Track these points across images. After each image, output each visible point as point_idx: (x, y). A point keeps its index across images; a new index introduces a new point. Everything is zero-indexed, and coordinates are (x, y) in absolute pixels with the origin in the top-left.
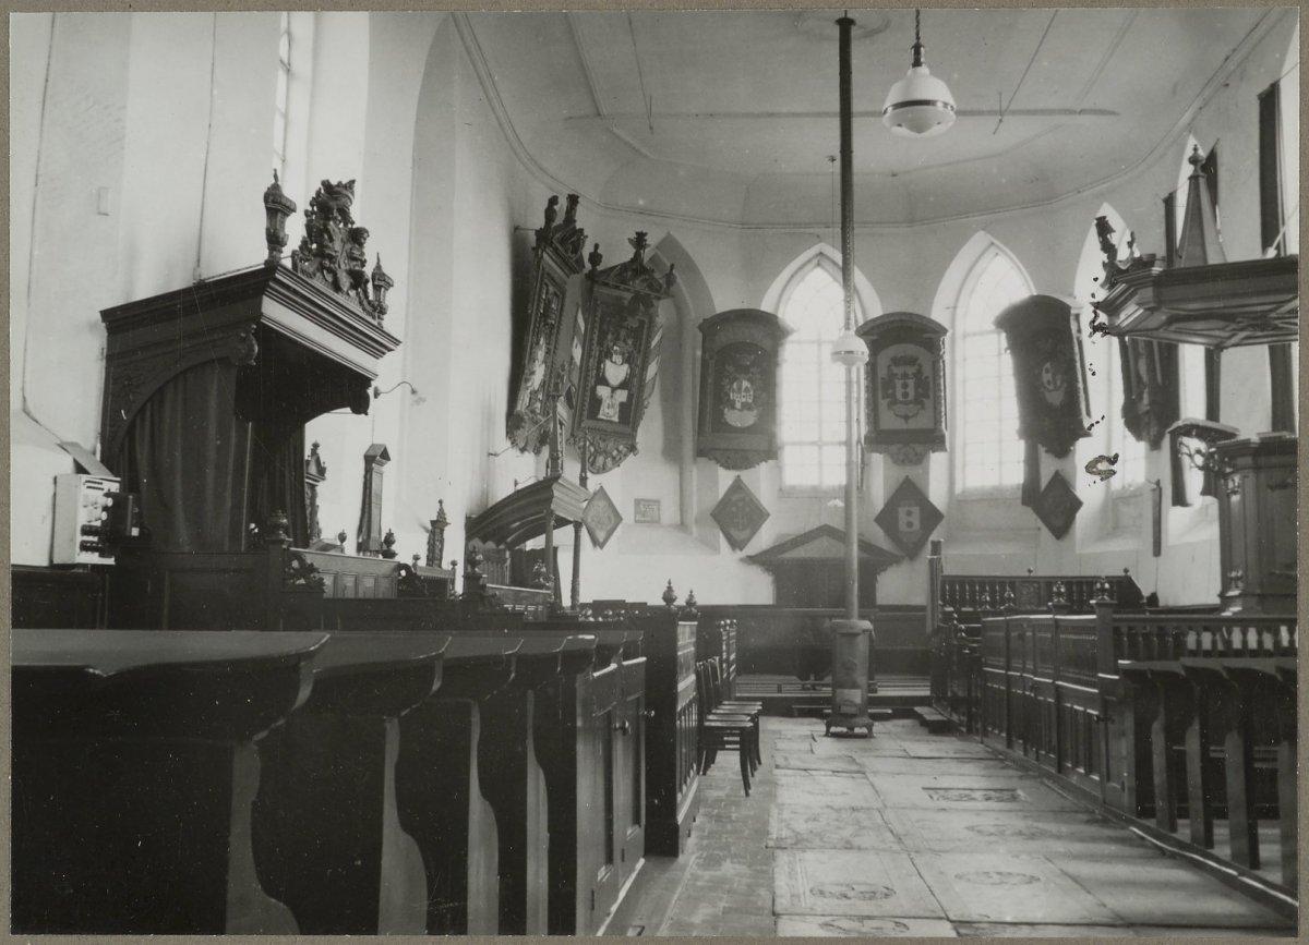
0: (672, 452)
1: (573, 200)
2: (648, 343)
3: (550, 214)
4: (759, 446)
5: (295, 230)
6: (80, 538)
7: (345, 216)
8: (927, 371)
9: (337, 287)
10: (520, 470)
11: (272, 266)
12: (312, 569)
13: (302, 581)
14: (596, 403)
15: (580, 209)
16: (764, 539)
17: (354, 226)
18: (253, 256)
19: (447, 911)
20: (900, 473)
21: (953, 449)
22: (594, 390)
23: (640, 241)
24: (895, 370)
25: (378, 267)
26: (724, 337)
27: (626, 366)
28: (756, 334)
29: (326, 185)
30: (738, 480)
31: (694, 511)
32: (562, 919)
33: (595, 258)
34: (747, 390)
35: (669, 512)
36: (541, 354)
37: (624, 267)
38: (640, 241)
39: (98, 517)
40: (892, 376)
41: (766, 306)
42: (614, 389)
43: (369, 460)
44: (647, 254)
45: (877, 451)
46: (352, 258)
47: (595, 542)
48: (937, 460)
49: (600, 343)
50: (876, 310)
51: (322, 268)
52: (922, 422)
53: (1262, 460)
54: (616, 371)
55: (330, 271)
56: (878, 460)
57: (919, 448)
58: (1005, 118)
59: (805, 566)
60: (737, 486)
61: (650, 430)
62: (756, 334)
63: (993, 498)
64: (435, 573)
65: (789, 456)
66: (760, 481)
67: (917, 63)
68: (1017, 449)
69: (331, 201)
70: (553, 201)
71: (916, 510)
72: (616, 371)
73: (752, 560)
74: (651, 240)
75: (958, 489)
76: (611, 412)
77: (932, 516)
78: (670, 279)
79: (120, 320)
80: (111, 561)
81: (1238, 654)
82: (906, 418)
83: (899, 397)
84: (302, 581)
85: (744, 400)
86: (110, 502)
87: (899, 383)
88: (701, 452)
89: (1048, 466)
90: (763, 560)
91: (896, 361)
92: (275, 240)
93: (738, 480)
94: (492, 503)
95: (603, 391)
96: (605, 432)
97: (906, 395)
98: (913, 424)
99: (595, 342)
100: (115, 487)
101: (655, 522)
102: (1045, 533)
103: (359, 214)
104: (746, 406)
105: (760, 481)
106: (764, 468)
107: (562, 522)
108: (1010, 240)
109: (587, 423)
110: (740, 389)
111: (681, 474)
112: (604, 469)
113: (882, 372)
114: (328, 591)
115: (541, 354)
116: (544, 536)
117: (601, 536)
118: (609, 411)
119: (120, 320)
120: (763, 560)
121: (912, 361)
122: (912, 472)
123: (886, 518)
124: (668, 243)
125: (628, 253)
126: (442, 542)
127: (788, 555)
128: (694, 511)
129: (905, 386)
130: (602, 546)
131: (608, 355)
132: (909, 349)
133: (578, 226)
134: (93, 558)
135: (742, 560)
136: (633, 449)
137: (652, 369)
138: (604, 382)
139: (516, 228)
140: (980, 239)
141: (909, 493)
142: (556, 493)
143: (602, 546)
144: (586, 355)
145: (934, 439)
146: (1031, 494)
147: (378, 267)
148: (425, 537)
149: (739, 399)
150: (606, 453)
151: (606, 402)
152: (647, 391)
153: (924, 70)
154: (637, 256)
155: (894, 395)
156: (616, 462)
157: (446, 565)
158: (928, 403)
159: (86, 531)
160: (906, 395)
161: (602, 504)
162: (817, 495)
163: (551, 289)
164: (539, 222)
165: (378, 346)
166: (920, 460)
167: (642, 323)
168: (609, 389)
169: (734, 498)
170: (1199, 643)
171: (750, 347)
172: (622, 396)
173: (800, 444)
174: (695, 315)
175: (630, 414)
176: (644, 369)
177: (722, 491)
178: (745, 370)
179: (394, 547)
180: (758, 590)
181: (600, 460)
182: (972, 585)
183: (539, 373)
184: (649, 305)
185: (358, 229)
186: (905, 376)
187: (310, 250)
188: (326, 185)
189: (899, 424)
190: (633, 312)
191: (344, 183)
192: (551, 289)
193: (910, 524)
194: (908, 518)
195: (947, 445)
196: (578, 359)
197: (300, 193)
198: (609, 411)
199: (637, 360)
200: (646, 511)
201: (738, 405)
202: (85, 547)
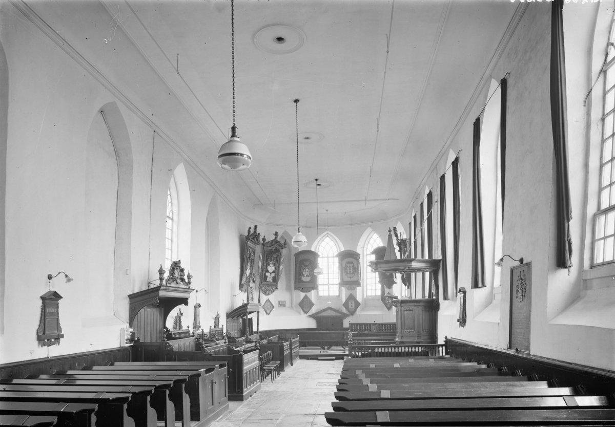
0: (288, 289)
1: (256, 227)
2: (280, 260)
3: (249, 232)
4: (312, 285)
5: (166, 275)
6: (125, 341)
8: (355, 265)
10: (240, 299)
11: (161, 285)
14: (266, 277)
15: (258, 228)
16: (313, 310)
19: (179, 417)
20: (349, 292)
21: (363, 286)
22: (265, 274)
23: (276, 234)
24: (348, 265)
26: (302, 257)
27: (274, 267)
28: (306, 257)
30: (306, 296)
31: (294, 304)
32: (195, 416)
33: (264, 240)
35: (288, 304)
36: (249, 267)
37: (272, 241)
38: (276, 234)
39: (129, 337)
40: (346, 267)
41: (313, 249)
42: (271, 273)
43: (195, 307)
44: (278, 238)
45: (343, 287)
48: (359, 289)
49: (267, 262)
50: (343, 249)
51: (173, 281)
52: (355, 279)
53: (402, 305)
54: (271, 268)
56: (343, 289)
57: (354, 286)
58: (367, 202)
59: (327, 318)
60: (306, 297)
61: (281, 283)
62: (306, 257)
63: (373, 298)
64: (217, 329)
65: (320, 288)
66: (312, 295)
67: (299, 232)
68: (379, 286)
69: (176, 265)
70: (250, 228)
71: (353, 302)
73: (310, 316)
74: (280, 234)
75: (365, 296)
76: (270, 279)
77: (357, 304)
78: (285, 243)
79: (132, 297)
80: (132, 344)
81: (420, 346)
82: (350, 278)
83: (349, 272)
86: (131, 334)
87: (348, 269)
88: (295, 288)
89: (387, 290)
90: (313, 316)
91: (348, 263)
92: (161, 279)
93: (306, 296)
94: (235, 308)
95: (267, 274)
96: (269, 285)
98: (352, 279)
100: (132, 330)
101: (284, 306)
102: (385, 308)
103: (182, 265)
104: (307, 276)
105: (312, 295)
106: (313, 292)
108: (375, 229)
109: (264, 283)
111: (291, 295)
112: (269, 294)
113: (344, 266)
114: (174, 350)
115: (249, 267)
117: (268, 312)
118: (270, 279)
119: (132, 297)
120: (313, 316)
121: (352, 263)
123: (346, 305)
124: (285, 233)
125: (273, 237)
126: (218, 321)
127: (319, 315)
128: (294, 304)
129: (350, 269)
130: (269, 314)
131: (269, 264)
132: (351, 260)
133: (258, 232)
134: (129, 345)
135: (307, 317)
136: (277, 288)
137: (281, 267)
138: (268, 271)
139: (241, 235)
140: (369, 229)
141: (352, 298)
143: (269, 314)
145: (358, 283)
146: (383, 298)
148: (213, 321)
149: (305, 274)
150: (269, 290)
151: (269, 277)
152: (280, 273)
153: (300, 233)
154: (276, 238)
155: (347, 272)
156: (272, 292)
157: (220, 326)
158: (356, 274)
159: (127, 340)
160: (350, 272)
161: (269, 303)
162: (329, 298)
163: (251, 250)
164: (246, 234)
165: (190, 290)
166: (354, 289)
167: (278, 255)
168: (269, 274)
169: (305, 300)
171: (306, 260)
172: (273, 275)
173: (323, 285)
174: (294, 252)
175: (275, 280)
176: (279, 267)
177: (302, 298)
178: (307, 266)
180: (311, 324)
181: (268, 292)
182: (367, 325)
183: (248, 272)
184: (278, 251)
186: (350, 266)
189: (349, 279)
190: (275, 253)
193: (352, 306)
194: (352, 305)
195: (361, 285)
196: (260, 266)
197: (167, 267)
198: (270, 279)
199: (277, 264)
200: (282, 304)
202: (126, 343)
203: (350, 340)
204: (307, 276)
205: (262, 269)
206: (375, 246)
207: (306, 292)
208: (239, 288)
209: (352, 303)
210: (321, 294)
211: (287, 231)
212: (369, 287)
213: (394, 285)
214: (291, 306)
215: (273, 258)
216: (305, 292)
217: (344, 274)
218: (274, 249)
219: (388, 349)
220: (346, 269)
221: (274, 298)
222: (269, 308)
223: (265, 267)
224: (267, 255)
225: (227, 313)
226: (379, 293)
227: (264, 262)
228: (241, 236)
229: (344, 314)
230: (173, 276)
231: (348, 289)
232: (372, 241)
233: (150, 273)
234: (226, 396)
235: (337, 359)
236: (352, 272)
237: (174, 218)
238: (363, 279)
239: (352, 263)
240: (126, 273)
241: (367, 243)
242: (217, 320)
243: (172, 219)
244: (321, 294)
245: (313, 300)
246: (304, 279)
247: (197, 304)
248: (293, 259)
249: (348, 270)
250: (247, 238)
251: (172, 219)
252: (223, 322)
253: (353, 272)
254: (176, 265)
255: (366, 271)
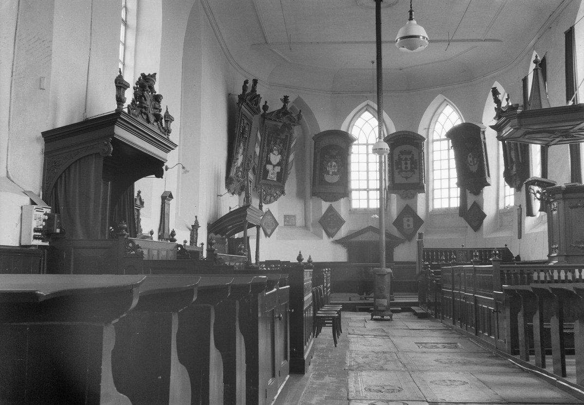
0: (301, 194)
1: (255, 82)
2: (290, 145)
3: (245, 88)
4: (342, 190)
5: (129, 95)
6: (33, 234)
7: (151, 88)
8: (416, 157)
9: (148, 121)
10: (231, 203)
11: (119, 112)
12: (138, 247)
13: (134, 252)
14: (266, 172)
16: (343, 232)
17: (156, 94)
18: (110, 107)
20: (404, 203)
22: (265, 166)
23: (285, 99)
24: (403, 157)
25: (167, 112)
27: (280, 156)
29: (143, 75)
31: (311, 219)
33: (265, 107)
34: (334, 166)
35: (300, 221)
36: (241, 151)
37: (279, 111)
38: (285, 99)
39: (41, 224)
40: (400, 159)
41: (343, 128)
42: (274, 166)
44: (289, 106)
46: (155, 108)
47: (267, 235)
49: (268, 145)
50: (393, 130)
52: (414, 180)
53: (567, 196)
54: (275, 158)
55: (145, 114)
56: (394, 197)
57: (413, 191)
60: (331, 209)
61: (291, 185)
65: (354, 195)
66: (341, 207)
67: (411, 19)
68: (456, 192)
69: (146, 82)
70: (246, 82)
71: (411, 219)
72: (275, 158)
73: (337, 242)
74: (291, 99)
75: (430, 209)
76: (273, 176)
77: (418, 222)
78: (299, 117)
79: (50, 137)
80: (47, 244)
82: (407, 178)
84: (134, 252)
85: (333, 171)
87: (403, 163)
91: (402, 153)
92: (120, 100)
94: (219, 217)
95: (269, 167)
96: (270, 185)
97: (406, 168)
98: (410, 181)
99: (265, 145)
101: (293, 225)
104: (334, 173)
105: (341, 207)
106: (342, 201)
107: (251, 226)
109: (262, 181)
110: (331, 166)
112: (270, 202)
113: (396, 158)
114: (146, 257)
115: (241, 151)
116: (243, 232)
117: (269, 232)
118: (272, 176)
119: (50, 137)
121: (409, 153)
122: (409, 202)
123: (398, 223)
124: (298, 101)
125: (280, 105)
128: (311, 219)
129: (406, 164)
131: (271, 151)
134: (39, 242)
136: (283, 193)
137: (291, 157)
138: (270, 163)
139: (229, 94)
140: (439, 98)
141: (408, 211)
142: (248, 213)
144: (262, 151)
147: (167, 112)
148: (189, 233)
149: (331, 170)
150: (271, 195)
151: (271, 172)
153: (414, 22)
154: (284, 106)
156: (276, 199)
157: (199, 245)
158: (417, 171)
159: (36, 230)
160: (406, 168)
161: (269, 217)
162: (367, 212)
163: (246, 121)
164: (240, 91)
165: (168, 147)
166: (414, 197)
167: (287, 136)
170: (539, 277)
172: (278, 169)
173: (359, 190)
175: (282, 177)
176: (288, 157)
177: (324, 210)
179: (175, 237)
180: (340, 255)
181: (268, 197)
183: (240, 159)
185: (157, 95)
186: (406, 159)
187: (136, 105)
188: (143, 75)
189: (404, 181)
191: (151, 74)
192: (246, 121)
193: (409, 225)
196: (258, 153)
197: (131, 79)
198: (272, 176)
199: (285, 152)
200: (289, 220)
201: (331, 173)
202: (35, 238)
203: (495, 254)
204: (334, 173)
205: (261, 157)
206: (449, 127)
207: (332, 201)
208: (225, 186)
209: (408, 221)
210: (355, 205)
211: (301, 96)
212: (437, 194)
213: (486, 188)
214: (305, 226)
215: (278, 141)
216: (329, 201)
217: (396, 172)
218: (281, 124)
219: (539, 277)
220: (399, 163)
221: (276, 208)
222: (269, 226)
223: (264, 154)
224: (269, 135)
225: (208, 224)
226: (456, 203)
227: (264, 146)
228: (229, 98)
229: (396, 238)
230: (141, 103)
231: (403, 197)
232: (442, 118)
233: (89, 102)
234: (286, 358)
235: (403, 310)
236: (409, 168)
237: (128, 23)
238: (428, 181)
239: (409, 153)
240: (40, 86)
241: (433, 121)
242: (195, 229)
243: (126, 24)
244: (355, 205)
245: (343, 213)
246: (328, 178)
247: (165, 192)
248: (310, 144)
249: (403, 167)
250: (242, 98)
251: (126, 24)
252: (202, 237)
253: (411, 168)
254: (146, 82)
255: (433, 168)
